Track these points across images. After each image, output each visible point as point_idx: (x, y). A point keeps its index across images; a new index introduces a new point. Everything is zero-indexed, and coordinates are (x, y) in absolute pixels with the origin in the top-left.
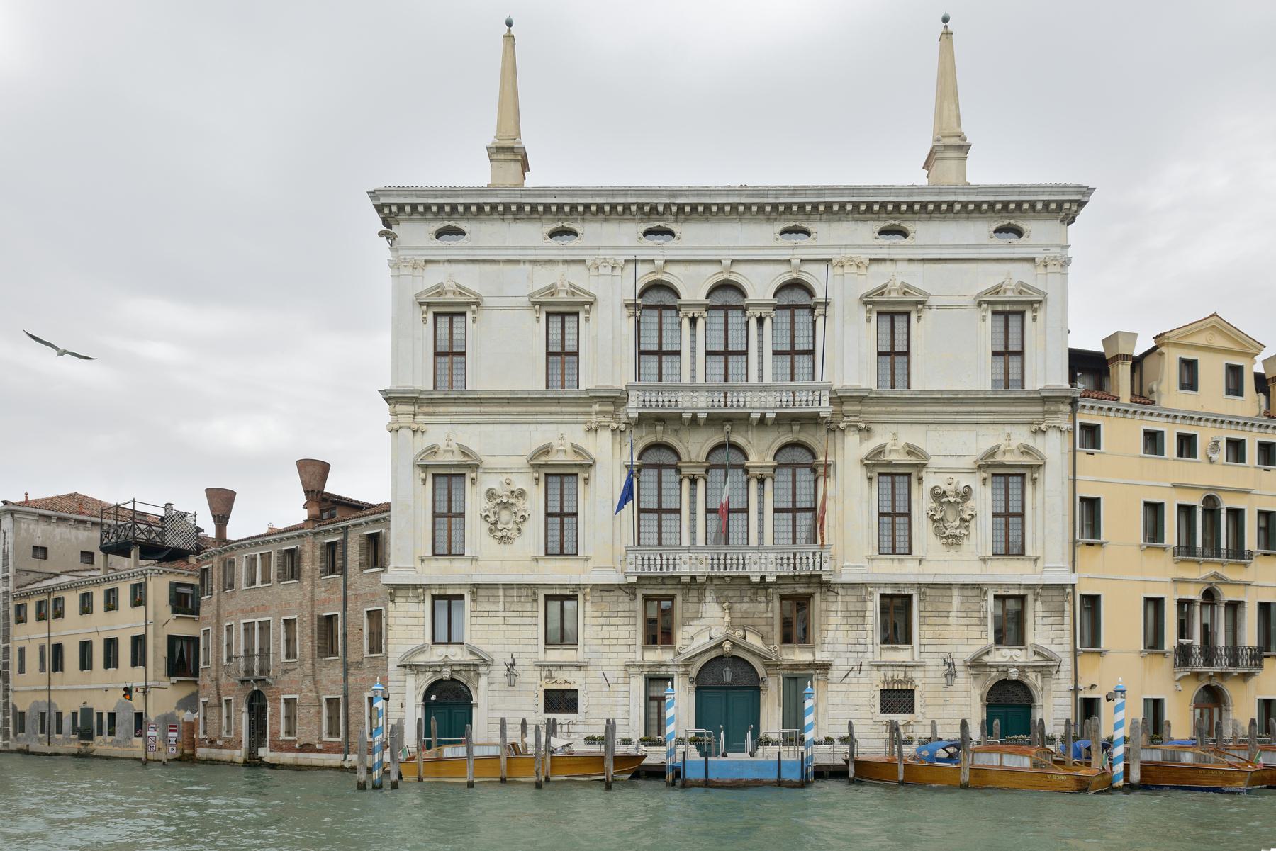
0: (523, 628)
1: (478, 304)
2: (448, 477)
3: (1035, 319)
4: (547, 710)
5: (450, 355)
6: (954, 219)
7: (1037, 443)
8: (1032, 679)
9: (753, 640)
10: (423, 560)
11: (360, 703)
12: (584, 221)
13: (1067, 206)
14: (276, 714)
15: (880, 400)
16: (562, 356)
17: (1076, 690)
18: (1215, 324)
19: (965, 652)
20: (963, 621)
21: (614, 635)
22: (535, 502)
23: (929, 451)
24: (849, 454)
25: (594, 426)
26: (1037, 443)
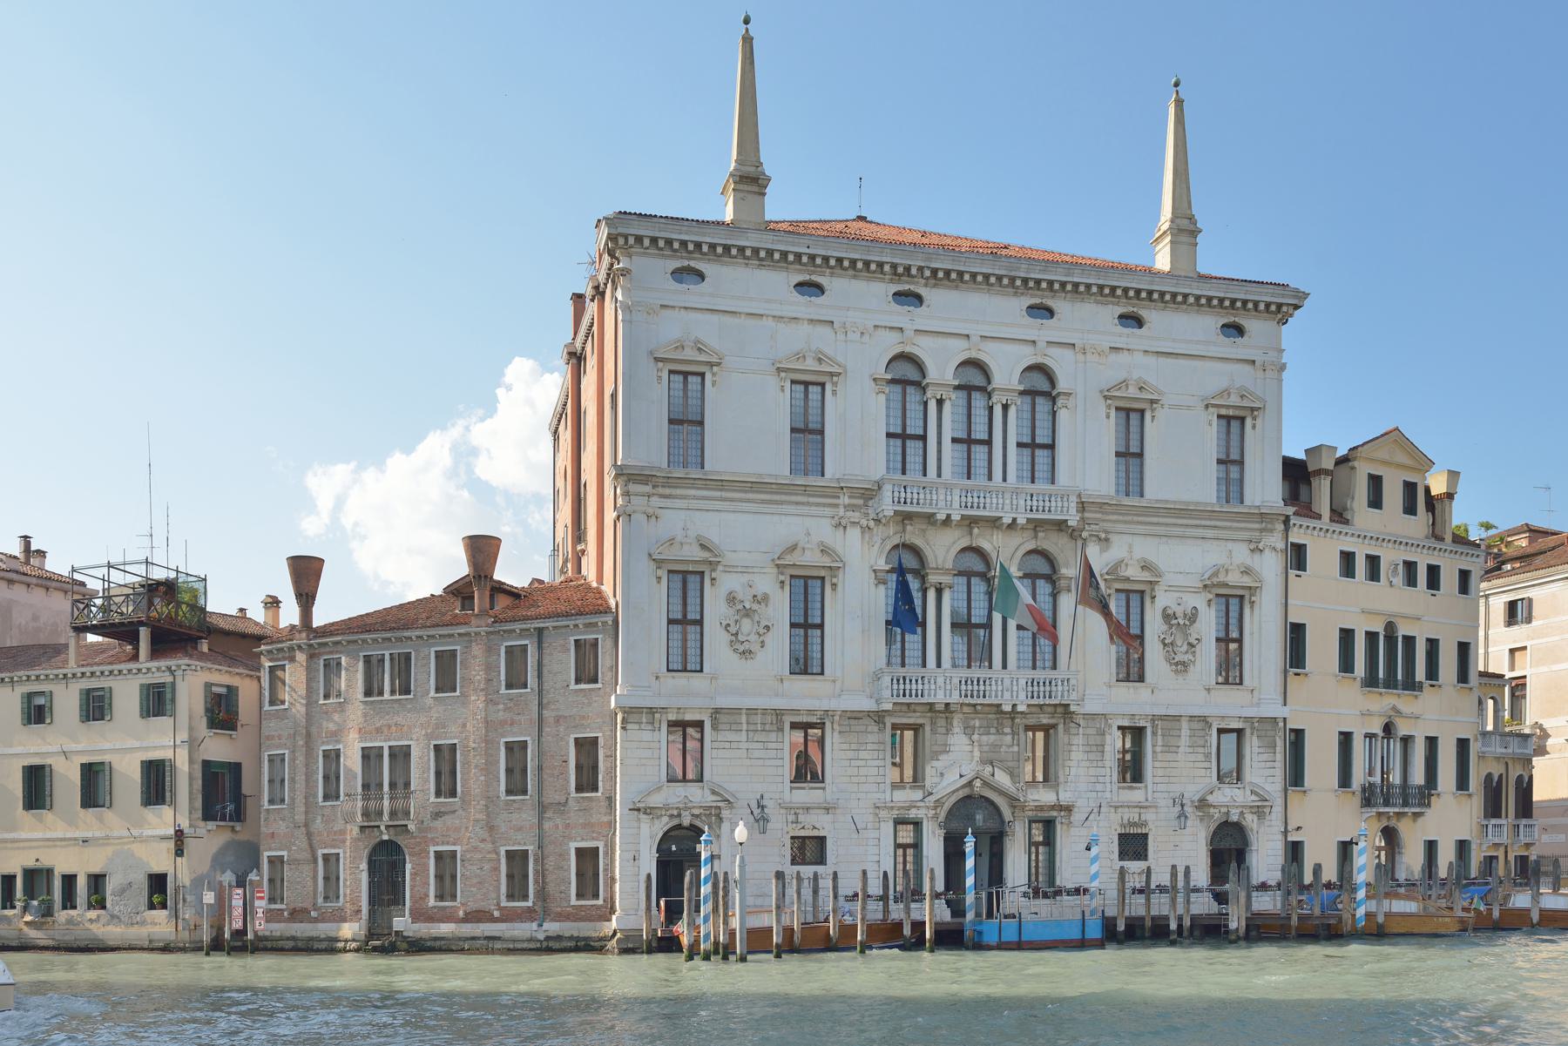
0: (768, 762)
2: (687, 580)
3: (1254, 427)
4: (1121, 859)
5: (687, 422)
6: (1185, 311)
7: (1255, 562)
8: (1250, 821)
9: (1002, 779)
11: (563, 856)
12: (832, 275)
13: (1284, 309)
14: (421, 871)
15: (1118, 508)
16: (808, 433)
17: (1286, 833)
18: (1394, 437)
19: (1192, 792)
20: (1192, 757)
21: (863, 771)
22: (780, 610)
23: (1162, 566)
25: (844, 522)
26: (1255, 562)
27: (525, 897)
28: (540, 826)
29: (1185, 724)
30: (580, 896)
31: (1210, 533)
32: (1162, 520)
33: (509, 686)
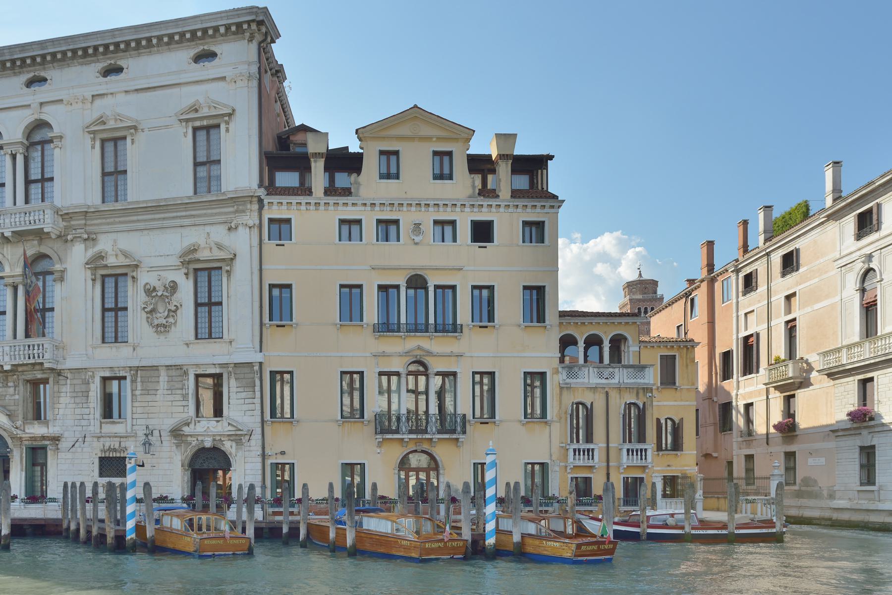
1: (135, 128)
3: (227, 130)
8: (228, 447)
10: (187, 344)
16: (206, 165)
20: (171, 398)
24: (75, 258)
29: (163, 373)
31: (187, 222)
32: (140, 218)
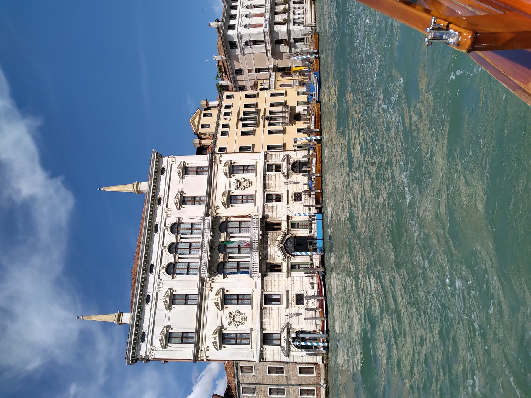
7: (223, 163)
8: (291, 161)
11: (302, 378)
16: (198, 170)
19: (284, 179)
27: (314, 390)
28: (293, 385)
30: (313, 373)
33: (254, 393)
